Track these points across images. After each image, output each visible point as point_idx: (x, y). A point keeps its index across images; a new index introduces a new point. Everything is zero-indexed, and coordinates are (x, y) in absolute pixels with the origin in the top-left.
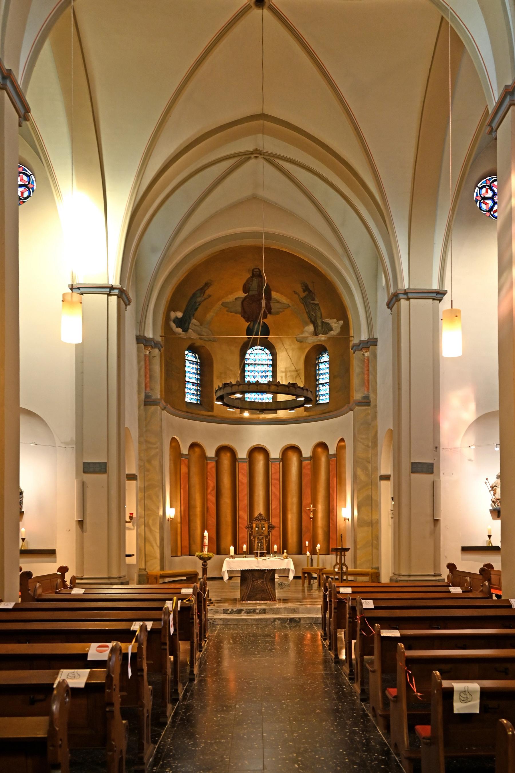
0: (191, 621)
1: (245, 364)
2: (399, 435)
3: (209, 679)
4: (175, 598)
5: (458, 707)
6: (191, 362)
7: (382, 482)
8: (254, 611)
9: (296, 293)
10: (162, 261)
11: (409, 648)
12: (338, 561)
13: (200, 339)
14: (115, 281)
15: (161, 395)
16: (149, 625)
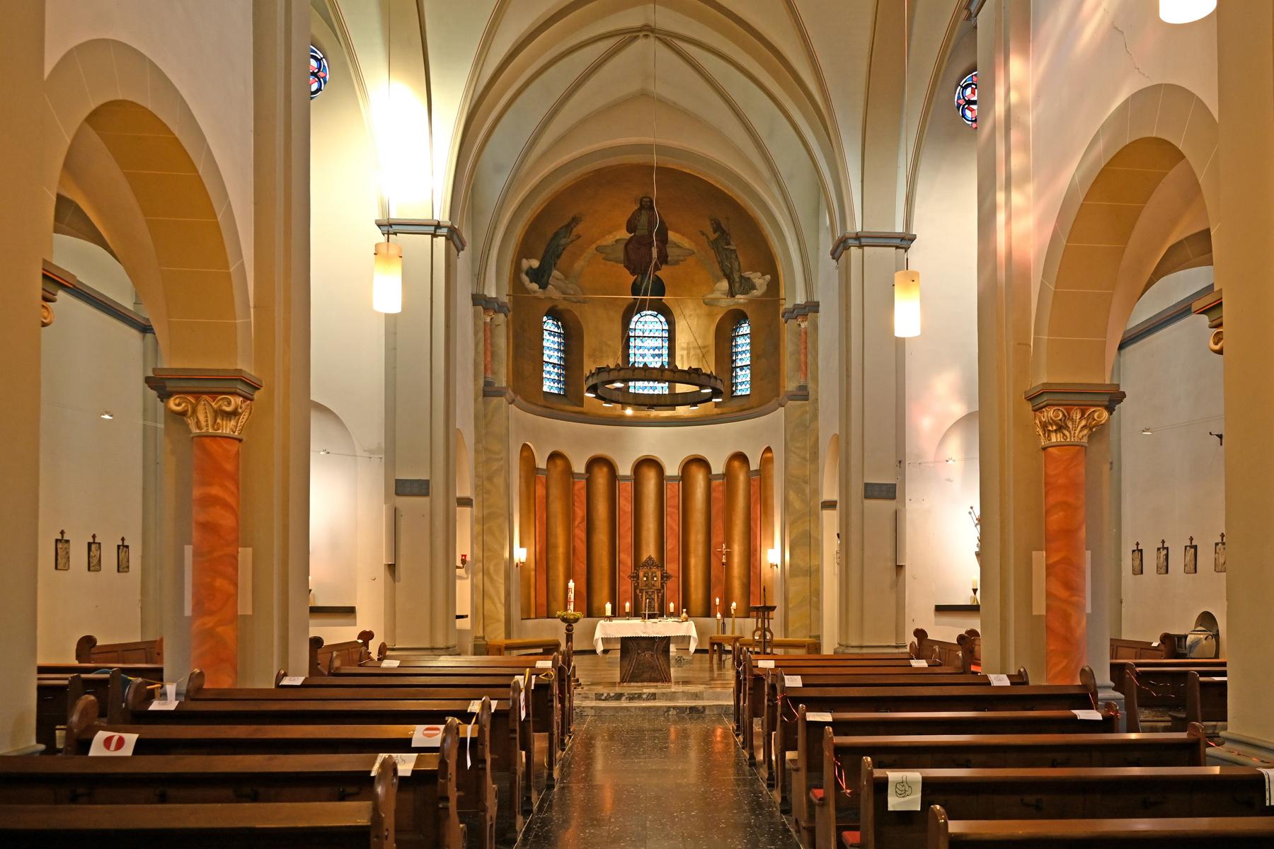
1: (629, 337)
2: (848, 443)
3: (574, 786)
5: (895, 803)
6: (550, 333)
9: (703, 234)
11: (836, 734)
14: (442, 215)
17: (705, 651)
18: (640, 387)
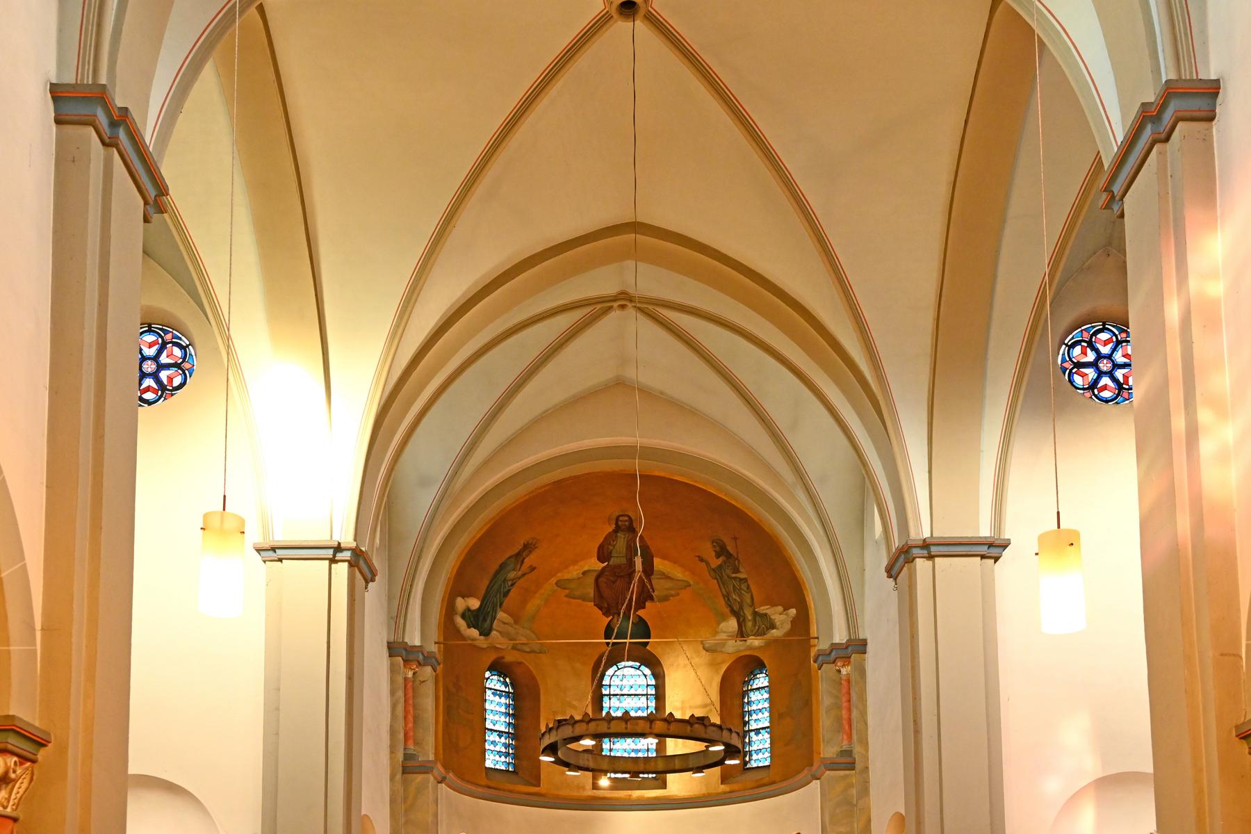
9: (702, 560)
10: (440, 501)
13: (514, 648)
14: (348, 539)
15: (436, 754)
18: (623, 747)
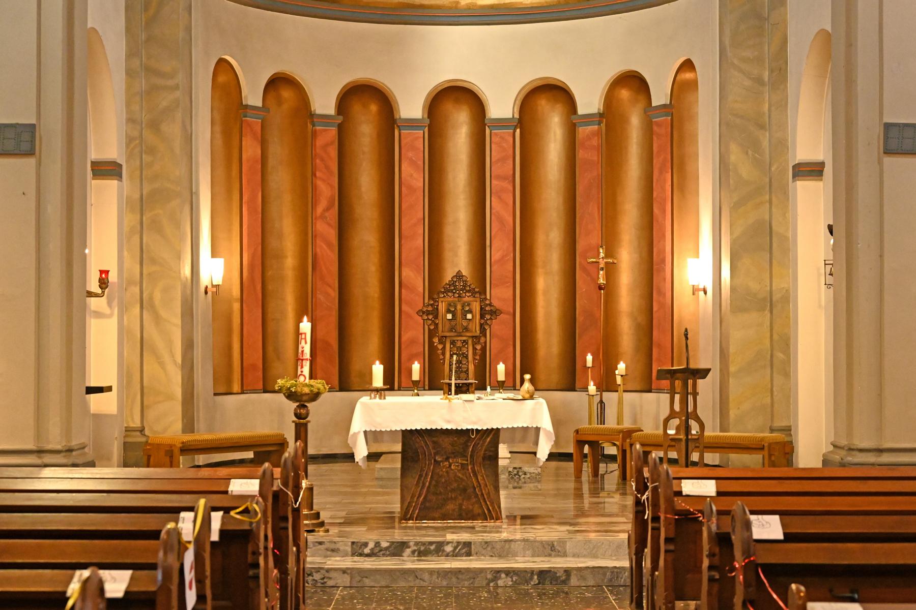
0: (251, 573)
2: (850, 45)
4: (202, 502)
7: (799, 184)
8: (439, 549)
12: (677, 407)
16: (116, 584)
17: (567, 457)
